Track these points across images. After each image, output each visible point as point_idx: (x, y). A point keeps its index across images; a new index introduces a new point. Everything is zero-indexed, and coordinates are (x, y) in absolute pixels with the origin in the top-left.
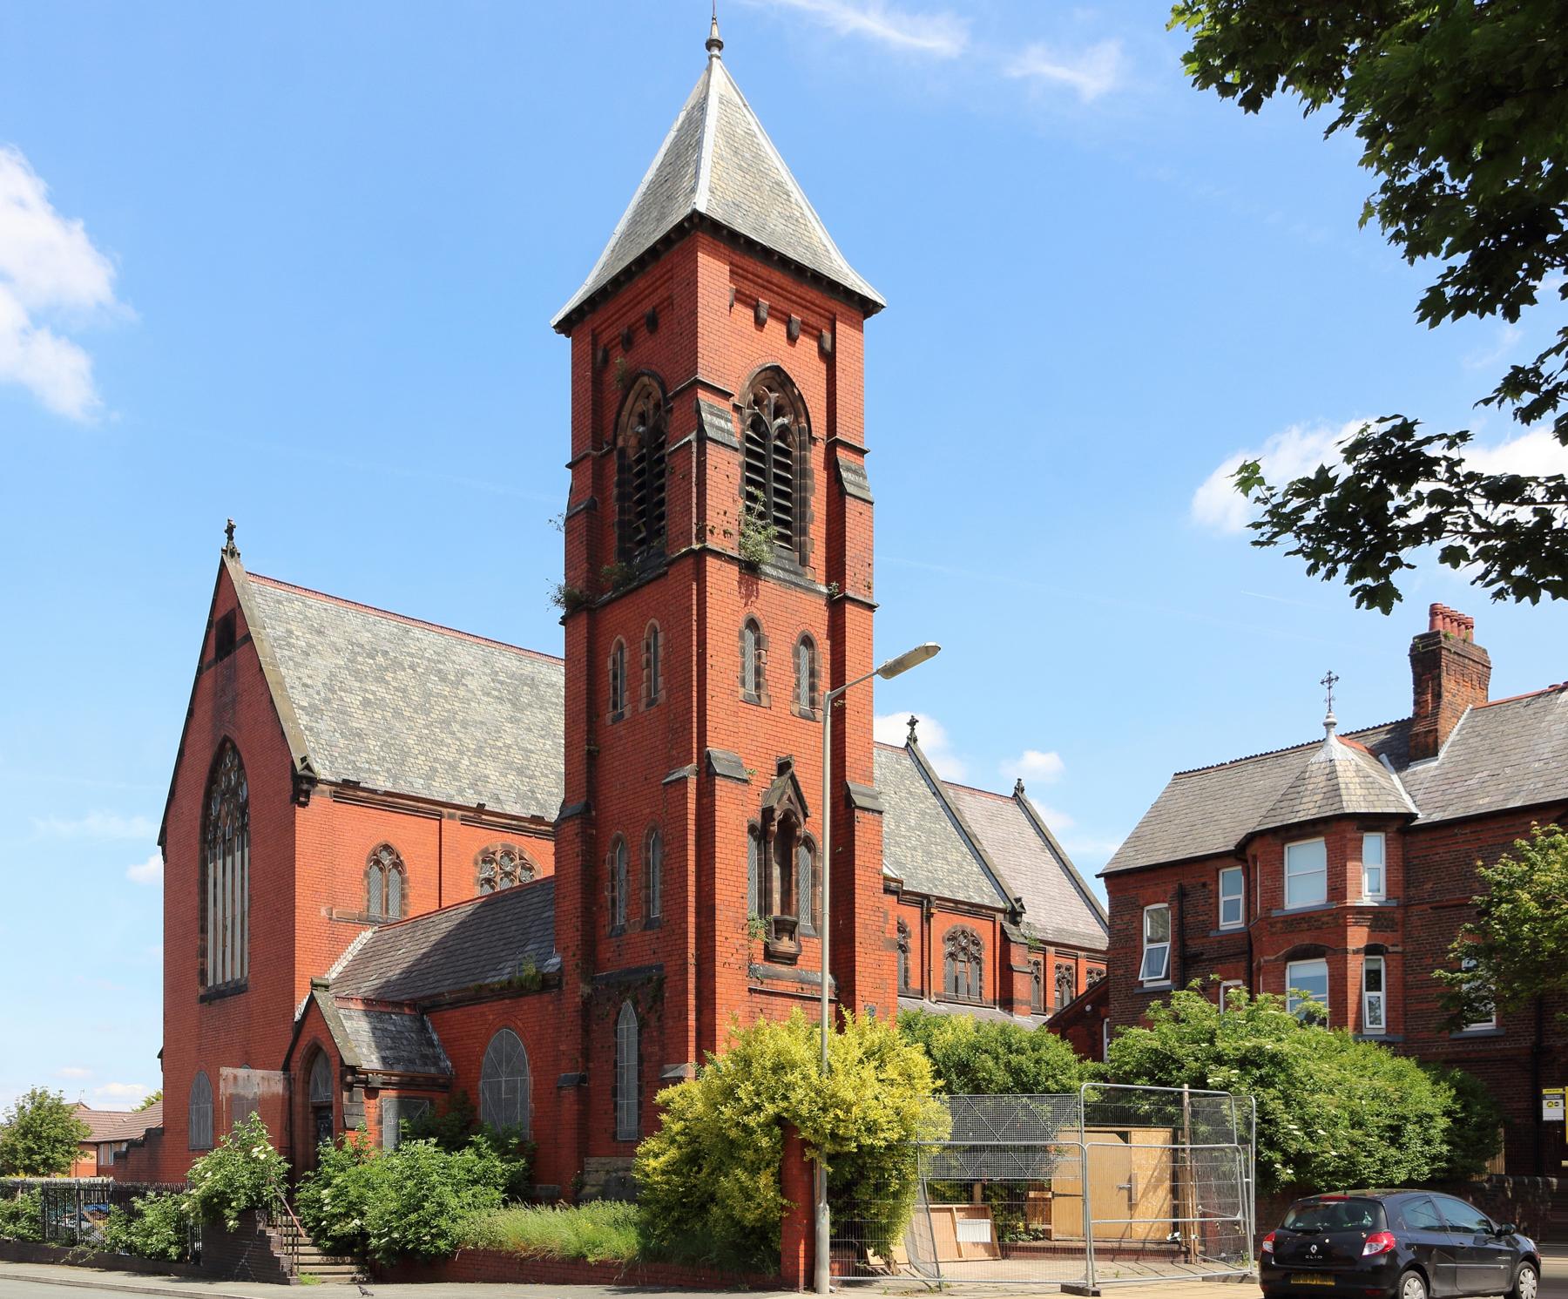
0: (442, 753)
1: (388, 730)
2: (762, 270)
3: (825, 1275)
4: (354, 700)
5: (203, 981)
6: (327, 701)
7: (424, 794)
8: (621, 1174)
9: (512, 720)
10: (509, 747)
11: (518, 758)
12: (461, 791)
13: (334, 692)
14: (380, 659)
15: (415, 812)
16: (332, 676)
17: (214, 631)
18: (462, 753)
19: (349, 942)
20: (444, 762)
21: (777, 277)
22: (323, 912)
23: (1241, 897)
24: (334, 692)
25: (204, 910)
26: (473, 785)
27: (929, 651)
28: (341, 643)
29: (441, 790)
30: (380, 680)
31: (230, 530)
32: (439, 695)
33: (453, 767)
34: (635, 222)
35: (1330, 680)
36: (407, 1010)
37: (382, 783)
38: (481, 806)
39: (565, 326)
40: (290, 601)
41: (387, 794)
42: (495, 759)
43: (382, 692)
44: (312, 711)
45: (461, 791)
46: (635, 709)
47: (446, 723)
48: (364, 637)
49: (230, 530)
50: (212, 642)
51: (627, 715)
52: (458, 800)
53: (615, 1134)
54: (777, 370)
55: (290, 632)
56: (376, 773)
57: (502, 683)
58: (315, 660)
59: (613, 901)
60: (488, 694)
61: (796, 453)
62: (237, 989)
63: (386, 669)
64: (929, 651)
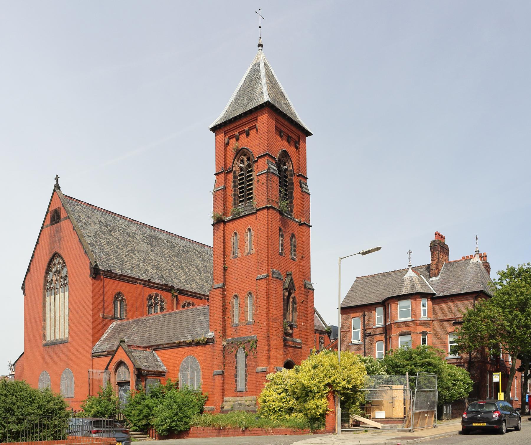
0: (134, 261)
1: (116, 253)
2: (282, 120)
3: (339, 428)
4: (104, 242)
5: (45, 339)
6: (96, 242)
7: (131, 275)
8: (239, 402)
9: (153, 251)
10: (152, 260)
11: (156, 263)
12: (142, 275)
13: (97, 239)
14: (109, 227)
15: (128, 281)
16: (96, 233)
17: (49, 214)
18: (139, 261)
19: (109, 326)
20: (135, 264)
21: (286, 123)
22: (101, 315)
23: (383, 316)
24: (97, 239)
25: (45, 313)
26: (145, 273)
27: (378, 249)
28: (96, 221)
29: (136, 274)
30: (110, 235)
31: (57, 178)
32: (128, 241)
33: (138, 266)
34: (238, 98)
35: (410, 253)
36: (148, 350)
37: (118, 271)
38: (149, 280)
39: (214, 129)
40: (78, 205)
41: (121, 275)
42: (149, 264)
43: (111, 239)
44: (92, 245)
45: (142, 275)
46: (242, 255)
47: (133, 251)
48: (102, 219)
49: (57, 178)
50: (49, 218)
51: (239, 255)
52: (142, 278)
53: (236, 390)
54: (285, 151)
55: (80, 216)
56: (116, 267)
57: (146, 237)
58: (90, 227)
59: (233, 315)
60: (143, 241)
61: (289, 177)
62: (63, 342)
63: (111, 231)
64: (378, 249)
